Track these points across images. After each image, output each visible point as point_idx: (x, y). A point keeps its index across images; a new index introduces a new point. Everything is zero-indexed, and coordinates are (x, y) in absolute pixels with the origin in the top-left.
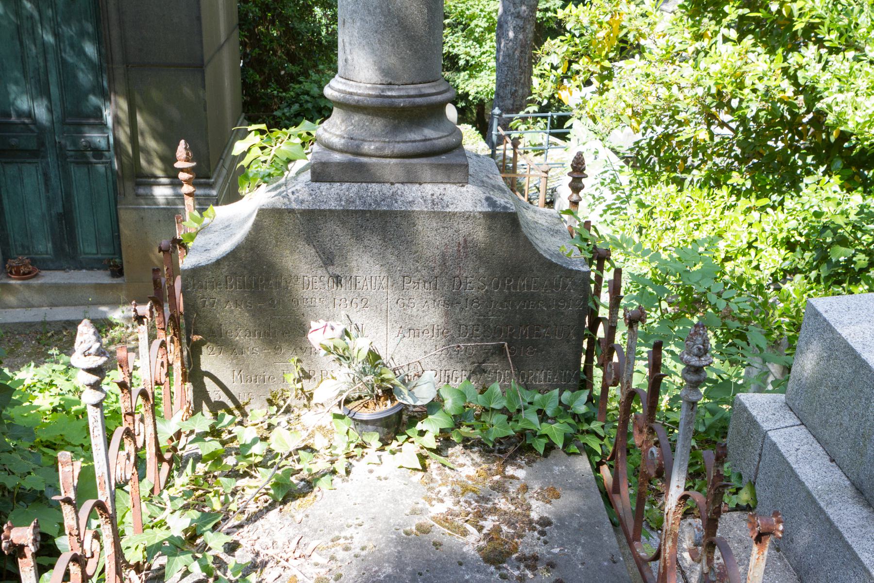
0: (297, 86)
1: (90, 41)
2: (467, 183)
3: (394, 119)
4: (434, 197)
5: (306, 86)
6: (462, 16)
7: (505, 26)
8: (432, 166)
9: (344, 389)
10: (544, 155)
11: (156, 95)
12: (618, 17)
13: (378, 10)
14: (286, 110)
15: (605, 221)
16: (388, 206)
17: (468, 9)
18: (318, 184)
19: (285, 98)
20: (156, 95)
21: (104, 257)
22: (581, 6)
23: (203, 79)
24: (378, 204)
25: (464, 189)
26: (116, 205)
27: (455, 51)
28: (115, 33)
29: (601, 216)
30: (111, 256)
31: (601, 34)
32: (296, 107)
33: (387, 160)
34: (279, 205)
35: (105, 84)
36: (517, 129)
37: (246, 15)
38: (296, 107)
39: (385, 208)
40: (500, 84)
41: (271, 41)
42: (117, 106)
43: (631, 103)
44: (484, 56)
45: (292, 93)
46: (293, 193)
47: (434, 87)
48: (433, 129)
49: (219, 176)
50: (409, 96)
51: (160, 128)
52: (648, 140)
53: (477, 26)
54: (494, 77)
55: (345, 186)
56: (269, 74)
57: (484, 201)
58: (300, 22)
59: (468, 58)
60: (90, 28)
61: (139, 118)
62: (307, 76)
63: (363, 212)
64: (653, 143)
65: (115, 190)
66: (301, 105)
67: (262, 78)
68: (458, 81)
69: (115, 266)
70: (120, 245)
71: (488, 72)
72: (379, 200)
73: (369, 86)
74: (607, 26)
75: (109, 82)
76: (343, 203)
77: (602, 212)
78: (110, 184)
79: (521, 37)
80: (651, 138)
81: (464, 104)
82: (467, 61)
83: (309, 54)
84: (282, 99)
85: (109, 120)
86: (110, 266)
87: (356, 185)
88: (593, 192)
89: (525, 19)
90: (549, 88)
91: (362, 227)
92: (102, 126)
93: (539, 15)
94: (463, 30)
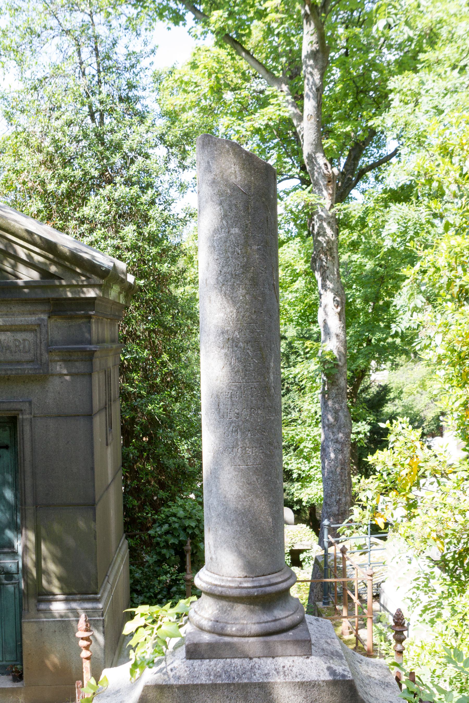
0: (166, 510)
1: (9, 488)
2: (311, 655)
3: (250, 604)
4: (285, 669)
5: (174, 509)
6: (293, 440)
7: (327, 449)
8: (282, 642)
9: (178, 515)
10: (367, 554)
11: (56, 527)
12: (415, 460)
13: (235, 522)
14: (158, 530)
15: (424, 620)
16: (248, 679)
17: (297, 435)
18: (191, 661)
19: (158, 519)
20: (56, 527)
21: (8, 663)
22: (385, 450)
23: (94, 515)
24: (240, 677)
25: (309, 660)
26: (21, 619)
27: (289, 467)
28: (29, 482)
29: (421, 615)
30: (14, 663)
31: (403, 473)
32: (166, 527)
33: (247, 639)
34: (160, 682)
35: (19, 521)
36: (343, 534)
37: (128, 455)
38: (166, 527)
39: (246, 681)
40: (327, 495)
41: (147, 474)
42: (27, 538)
43: (435, 529)
44: (312, 470)
45: (163, 515)
46: (172, 670)
47: (280, 576)
48: (281, 610)
49: (104, 591)
50: (261, 587)
51: (59, 554)
52: (452, 554)
53: (305, 447)
54: (321, 486)
55: (213, 662)
56: (145, 499)
57: (325, 671)
58: (168, 459)
59: (300, 472)
60: (10, 478)
61: (43, 547)
62: (174, 501)
63: (229, 685)
64: (457, 556)
65: (21, 606)
66: (170, 525)
67: (139, 502)
68: (293, 490)
69: (17, 671)
70: (21, 652)
71: (317, 483)
72: (240, 673)
73: (229, 579)
74: (408, 466)
75: (22, 520)
76: (212, 677)
77: (420, 613)
78: (17, 601)
79: (340, 457)
80: (455, 552)
81: (298, 508)
82: (299, 475)
83: (176, 481)
84: (154, 521)
85: (20, 549)
86: (13, 672)
87: (222, 661)
88: (411, 596)
89: (342, 444)
90: (367, 517)
91: (227, 697)
92: (15, 553)
93: (353, 436)
94: (294, 450)
